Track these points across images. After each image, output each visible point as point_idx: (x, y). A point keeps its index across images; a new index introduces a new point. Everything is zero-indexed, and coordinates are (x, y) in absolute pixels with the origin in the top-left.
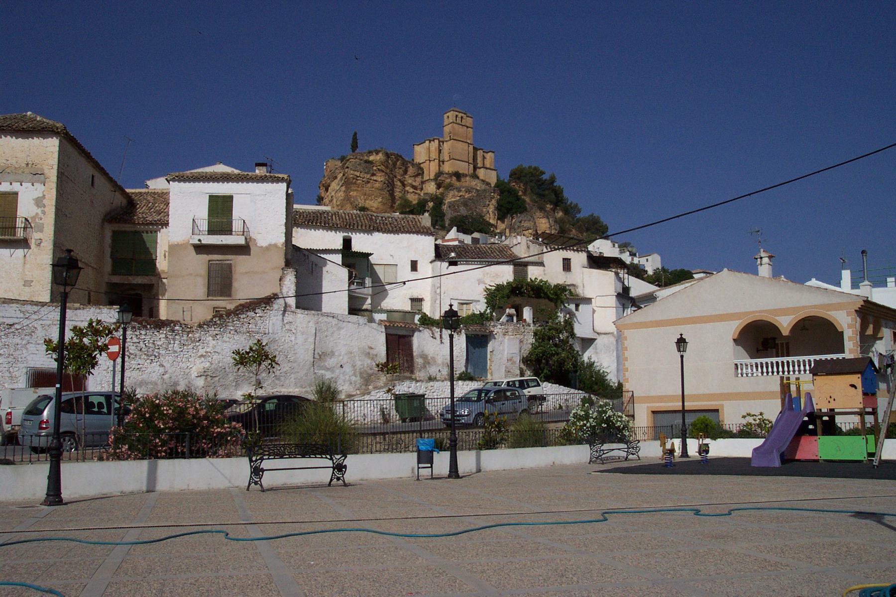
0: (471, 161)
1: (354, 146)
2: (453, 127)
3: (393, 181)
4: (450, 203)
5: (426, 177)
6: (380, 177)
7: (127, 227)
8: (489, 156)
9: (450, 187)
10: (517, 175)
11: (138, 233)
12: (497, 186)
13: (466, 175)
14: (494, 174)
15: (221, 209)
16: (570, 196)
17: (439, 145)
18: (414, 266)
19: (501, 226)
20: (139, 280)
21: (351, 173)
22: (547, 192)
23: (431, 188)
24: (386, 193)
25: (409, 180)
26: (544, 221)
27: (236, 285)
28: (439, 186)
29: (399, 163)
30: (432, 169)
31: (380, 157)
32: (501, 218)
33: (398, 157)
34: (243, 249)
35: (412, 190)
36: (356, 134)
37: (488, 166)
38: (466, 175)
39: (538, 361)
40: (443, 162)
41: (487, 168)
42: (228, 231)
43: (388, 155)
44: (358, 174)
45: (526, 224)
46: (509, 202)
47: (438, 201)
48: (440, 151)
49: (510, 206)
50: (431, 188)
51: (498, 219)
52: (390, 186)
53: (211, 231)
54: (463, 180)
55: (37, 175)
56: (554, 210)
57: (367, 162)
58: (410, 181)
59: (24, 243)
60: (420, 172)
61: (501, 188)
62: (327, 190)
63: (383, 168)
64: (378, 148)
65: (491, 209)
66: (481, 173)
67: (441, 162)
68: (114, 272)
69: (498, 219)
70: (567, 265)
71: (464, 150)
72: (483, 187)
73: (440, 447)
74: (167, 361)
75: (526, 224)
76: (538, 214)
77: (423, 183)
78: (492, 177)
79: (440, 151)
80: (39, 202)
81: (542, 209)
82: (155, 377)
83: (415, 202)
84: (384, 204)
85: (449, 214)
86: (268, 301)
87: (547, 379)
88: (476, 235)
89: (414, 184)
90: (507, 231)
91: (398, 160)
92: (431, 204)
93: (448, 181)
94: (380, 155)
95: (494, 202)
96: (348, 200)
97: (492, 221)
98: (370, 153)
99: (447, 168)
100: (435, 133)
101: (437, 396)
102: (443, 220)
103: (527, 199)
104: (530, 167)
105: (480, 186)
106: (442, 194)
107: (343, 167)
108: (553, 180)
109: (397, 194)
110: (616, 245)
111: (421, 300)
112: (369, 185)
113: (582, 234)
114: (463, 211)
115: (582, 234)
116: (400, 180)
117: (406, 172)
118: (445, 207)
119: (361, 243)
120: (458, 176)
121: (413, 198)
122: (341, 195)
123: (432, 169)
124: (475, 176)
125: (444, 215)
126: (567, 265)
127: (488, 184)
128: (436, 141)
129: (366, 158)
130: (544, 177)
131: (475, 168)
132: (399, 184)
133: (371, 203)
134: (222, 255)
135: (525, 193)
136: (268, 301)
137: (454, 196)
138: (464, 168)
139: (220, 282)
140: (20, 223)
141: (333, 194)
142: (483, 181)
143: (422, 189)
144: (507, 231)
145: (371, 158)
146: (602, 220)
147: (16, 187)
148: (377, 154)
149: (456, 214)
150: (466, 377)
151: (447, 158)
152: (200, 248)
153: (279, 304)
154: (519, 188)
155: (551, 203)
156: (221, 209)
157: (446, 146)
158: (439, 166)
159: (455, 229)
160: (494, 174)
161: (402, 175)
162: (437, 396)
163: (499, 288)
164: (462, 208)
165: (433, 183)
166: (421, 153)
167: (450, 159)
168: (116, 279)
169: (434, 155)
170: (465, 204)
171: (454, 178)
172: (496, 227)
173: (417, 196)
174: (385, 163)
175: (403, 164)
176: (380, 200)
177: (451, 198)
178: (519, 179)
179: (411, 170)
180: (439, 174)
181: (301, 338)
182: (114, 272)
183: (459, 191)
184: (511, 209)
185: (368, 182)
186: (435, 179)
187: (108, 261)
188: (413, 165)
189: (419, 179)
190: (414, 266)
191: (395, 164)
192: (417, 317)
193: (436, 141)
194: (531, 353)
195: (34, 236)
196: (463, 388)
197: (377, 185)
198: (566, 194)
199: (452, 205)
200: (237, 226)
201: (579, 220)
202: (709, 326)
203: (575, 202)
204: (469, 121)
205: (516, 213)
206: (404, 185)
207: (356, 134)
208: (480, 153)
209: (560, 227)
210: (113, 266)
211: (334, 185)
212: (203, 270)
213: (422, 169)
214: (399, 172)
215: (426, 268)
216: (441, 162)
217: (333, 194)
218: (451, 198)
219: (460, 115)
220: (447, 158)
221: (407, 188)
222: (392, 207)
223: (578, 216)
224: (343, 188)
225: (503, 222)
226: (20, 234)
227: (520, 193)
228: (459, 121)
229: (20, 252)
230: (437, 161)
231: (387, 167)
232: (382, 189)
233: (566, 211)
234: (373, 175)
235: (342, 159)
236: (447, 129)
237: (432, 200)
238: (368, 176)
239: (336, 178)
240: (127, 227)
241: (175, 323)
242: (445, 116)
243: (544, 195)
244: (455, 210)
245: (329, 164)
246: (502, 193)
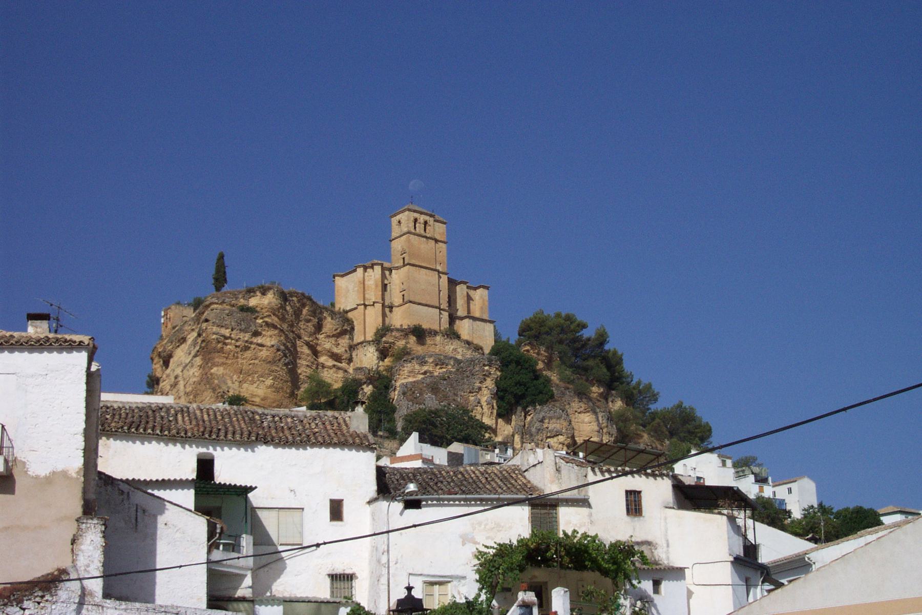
0: (444, 305)
2: (409, 241)
3: (294, 346)
4: (405, 386)
5: (358, 337)
6: (270, 339)
9: (404, 355)
10: (534, 330)
17: (383, 276)
18: (336, 511)
23: (368, 358)
24: (283, 372)
25: (326, 344)
26: (587, 417)
28: (383, 354)
30: (368, 322)
32: (505, 414)
35: (331, 362)
36: (221, 257)
40: (391, 308)
41: (475, 319)
44: (227, 332)
45: (553, 425)
47: (383, 382)
49: (520, 391)
50: (368, 358)
52: (289, 355)
54: (429, 341)
58: (328, 346)
60: (346, 327)
63: (274, 320)
65: (485, 396)
71: (430, 284)
75: (553, 425)
76: (576, 405)
77: (352, 348)
79: (384, 287)
83: (337, 385)
84: (277, 390)
85: (403, 408)
88: (457, 447)
89: (335, 350)
91: (304, 305)
92: (368, 389)
93: (401, 343)
95: (490, 383)
96: (208, 382)
97: (487, 421)
99: (399, 319)
104: (558, 315)
106: (389, 369)
108: (602, 339)
109: (304, 370)
112: (248, 354)
116: (307, 344)
117: (319, 328)
118: (395, 395)
119: (232, 465)
120: (420, 333)
122: (194, 373)
123: (368, 322)
125: (394, 410)
129: (242, 302)
131: (452, 319)
132: (306, 350)
133: (252, 388)
137: (412, 373)
138: (431, 319)
143: (350, 360)
145: (253, 302)
151: (397, 300)
155: (600, 382)
157: (396, 278)
158: (384, 315)
159: (415, 436)
161: (311, 335)
167: (404, 303)
169: (373, 295)
171: (413, 339)
173: (341, 374)
175: (314, 313)
176: (269, 382)
179: (330, 324)
180: (384, 330)
185: (247, 348)
189: (344, 341)
190: (336, 511)
191: (297, 313)
193: (378, 269)
197: (264, 353)
199: (409, 391)
205: (533, 403)
206: (315, 353)
207: (221, 257)
208: (461, 290)
213: (350, 322)
217: (178, 371)
219: (422, 218)
220: (397, 300)
221: (323, 359)
224: (198, 361)
228: (420, 229)
230: (379, 307)
231: (283, 319)
232: (273, 362)
234: (256, 334)
237: (370, 380)
238: (247, 336)
239: (184, 340)
242: (394, 220)
244: (415, 400)
246: (505, 365)
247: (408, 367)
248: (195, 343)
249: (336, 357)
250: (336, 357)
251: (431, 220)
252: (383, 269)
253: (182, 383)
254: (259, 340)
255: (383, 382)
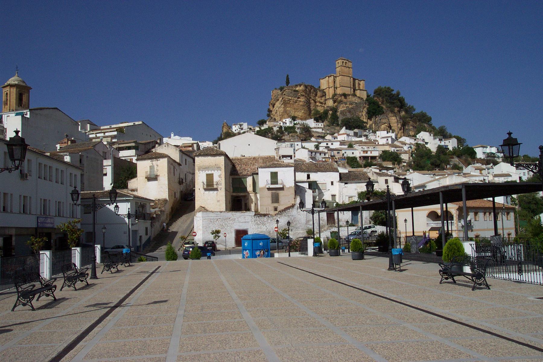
0: (352, 87)
1: (288, 83)
3: (309, 101)
4: (341, 111)
5: (327, 97)
6: (302, 99)
7: (237, 177)
8: (362, 83)
9: (341, 102)
10: (379, 92)
11: (240, 178)
12: (367, 100)
13: (350, 95)
14: (365, 92)
15: (274, 176)
16: (408, 102)
17: (334, 79)
19: (370, 122)
20: (242, 194)
21: (286, 98)
22: (395, 101)
23: (330, 103)
25: (318, 99)
26: (394, 118)
27: (280, 199)
29: (312, 91)
30: (330, 93)
31: (302, 88)
32: (370, 118)
33: (312, 87)
34: (282, 189)
35: (320, 105)
36: (288, 76)
37: (361, 88)
38: (350, 95)
39: (375, 218)
41: (361, 90)
42: (277, 183)
43: (306, 87)
44: (290, 98)
45: (384, 121)
46: (374, 109)
47: (335, 110)
48: (334, 82)
49: (374, 111)
50: (330, 103)
51: (368, 118)
52: (308, 103)
53: (272, 184)
54: (348, 97)
55: (219, 168)
56: (399, 111)
57: (295, 91)
58: (319, 100)
59: (216, 189)
60: (324, 94)
61: (369, 101)
62: (273, 107)
64: (300, 83)
66: (358, 93)
67: (335, 88)
68: (233, 192)
69: (368, 118)
70: (386, 181)
71: (348, 81)
72: (359, 101)
73: (346, 248)
74: (267, 225)
75: (384, 121)
76: (390, 114)
77: (325, 100)
78: (364, 95)
79: (334, 82)
80: (220, 176)
81: (392, 112)
82: (265, 230)
83: (322, 111)
85: (341, 118)
86: (293, 206)
87: (379, 224)
88: (356, 130)
90: (373, 125)
92: (331, 112)
93: (340, 98)
94: (302, 86)
95: (365, 109)
97: (365, 120)
98: (296, 86)
99: (339, 91)
100: (330, 71)
101: (344, 233)
102: (338, 121)
103: (384, 107)
104: (385, 87)
105: (357, 100)
106: (336, 106)
107: (282, 94)
108: (398, 94)
109: (312, 107)
110: (432, 135)
111: (335, 195)
112: (297, 104)
113: (416, 123)
114: (349, 116)
115: (416, 123)
117: (316, 95)
118: (338, 114)
119: (314, 177)
120: (345, 95)
121: (321, 109)
122: (282, 109)
123: (330, 93)
124: (354, 95)
126: (386, 181)
127: (362, 99)
128: (332, 77)
130: (393, 93)
131: (354, 90)
132: (313, 101)
134: (275, 192)
135: (382, 103)
136: (293, 206)
137: (343, 107)
138: (348, 91)
139: (276, 199)
140: (214, 183)
141: (277, 109)
142: (359, 97)
143: (325, 104)
144: (373, 125)
145: (297, 89)
146: (405, 100)
147: (213, 172)
148: (300, 86)
149: (345, 117)
150: (352, 225)
151: (338, 86)
152: (269, 189)
153: (296, 207)
154: (379, 100)
155: (398, 107)
156: (274, 176)
157: (338, 79)
158: (335, 91)
159: (344, 128)
160: (365, 92)
162: (344, 233)
163: (362, 193)
164: (348, 114)
165: (331, 100)
166: (324, 84)
168: (234, 194)
169: (331, 85)
170: (350, 112)
171: (343, 97)
172: (367, 123)
173: (323, 108)
174: (305, 91)
175: (314, 91)
176: (303, 111)
177: (341, 108)
178: (379, 94)
179: (319, 94)
180: (335, 95)
181: (302, 217)
182: (233, 192)
183: (346, 104)
184: (375, 113)
186: (333, 98)
187: (232, 188)
188: (320, 91)
189: (323, 98)
191: (310, 91)
192: (335, 204)
193: (332, 77)
194: (373, 216)
195: (219, 187)
196: (352, 229)
197: (301, 103)
198: (406, 101)
199: (342, 112)
200: (279, 181)
201: (414, 115)
202: (420, 212)
203: (411, 105)
204: (350, 64)
206: (315, 102)
207: (288, 76)
208: (357, 81)
209: (403, 121)
210: (233, 189)
211: (278, 104)
212: (270, 195)
213: (325, 93)
214: (312, 95)
215: (337, 184)
216: (335, 88)
217: (277, 109)
218: (341, 108)
219: (345, 61)
220: (338, 86)
221: (317, 104)
222: (309, 115)
223: (414, 113)
224: (283, 106)
225: (371, 120)
226: (215, 187)
227: (380, 103)
228: (344, 64)
229: (216, 192)
230: (333, 88)
231: (306, 93)
233: (406, 111)
234: (299, 98)
235: (281, 89)
236: (338, 70)
238: (296, 99)
239: (278, 100)
240: (237, 177)
241: (269, 214)
242: (337, 62)
243: (394, 103)
244: (344, 115)
245: (274, 92)
246: (370, 104)
247: (342, 105)
248: (281, 101)
249: (321, 103)
250: (321, 103)
251: (347, 62)
252: (334, 77)
253: (278, 113)
254: (300, 100)
255: (335, 110)
